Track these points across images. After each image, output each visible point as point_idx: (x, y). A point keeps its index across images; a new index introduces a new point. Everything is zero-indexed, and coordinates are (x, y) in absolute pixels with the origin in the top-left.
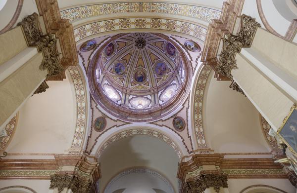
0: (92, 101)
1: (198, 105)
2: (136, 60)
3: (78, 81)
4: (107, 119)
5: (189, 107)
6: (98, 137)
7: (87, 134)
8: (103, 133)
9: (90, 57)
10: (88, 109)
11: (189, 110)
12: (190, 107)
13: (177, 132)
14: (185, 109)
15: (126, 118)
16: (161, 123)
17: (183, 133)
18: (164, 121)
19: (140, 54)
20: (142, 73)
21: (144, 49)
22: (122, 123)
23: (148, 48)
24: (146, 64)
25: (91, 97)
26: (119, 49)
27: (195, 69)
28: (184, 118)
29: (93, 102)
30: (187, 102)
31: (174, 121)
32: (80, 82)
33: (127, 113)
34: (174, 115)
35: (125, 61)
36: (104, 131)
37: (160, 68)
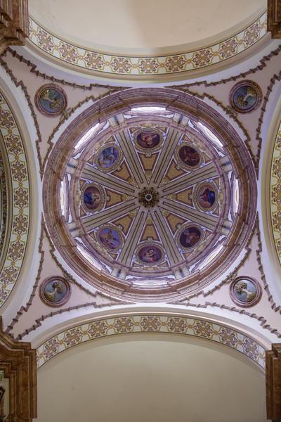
0: (106, 90)
1: (164, 324)
3: (162, 65)
4: (57, 120)
5: (100, 306)
6: (26, 92)
7: (44, 66)
8: (30, 105)
9: (210, 98)
10: (93, 77)
11: (92, 310)
13: (38, 289)
14: (92, 300)
15: (50, 167)
16: (46, 247)
17: (40, 308)
18: (53, 255)
21: (137, 203)
22: (43, 155)
24: (112, 209)
25: (116, 89)
28: (72, 302)
29: (102, 93)
30: (108, 302)
31: (58, 278)
32: (162, 71)
33: (60, 167)
34: (71, 277)
35: (119, 168)
36: (35, 108)
37: (110, 237)
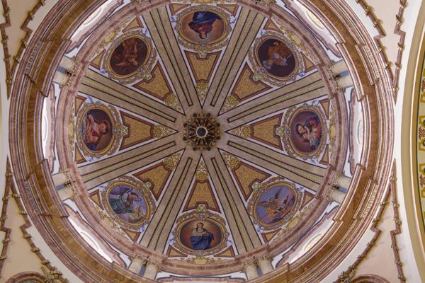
2: (188, 185)
5: (399, 224)
9: (29, 18)
11: (405, 239)
12: (405, 226)
19: (202, 170)
20: (206, 225)
23: (232, 125)
26: (127, 142)
27: (399, 65)
30: (390, 210)
37: (273, 204)
